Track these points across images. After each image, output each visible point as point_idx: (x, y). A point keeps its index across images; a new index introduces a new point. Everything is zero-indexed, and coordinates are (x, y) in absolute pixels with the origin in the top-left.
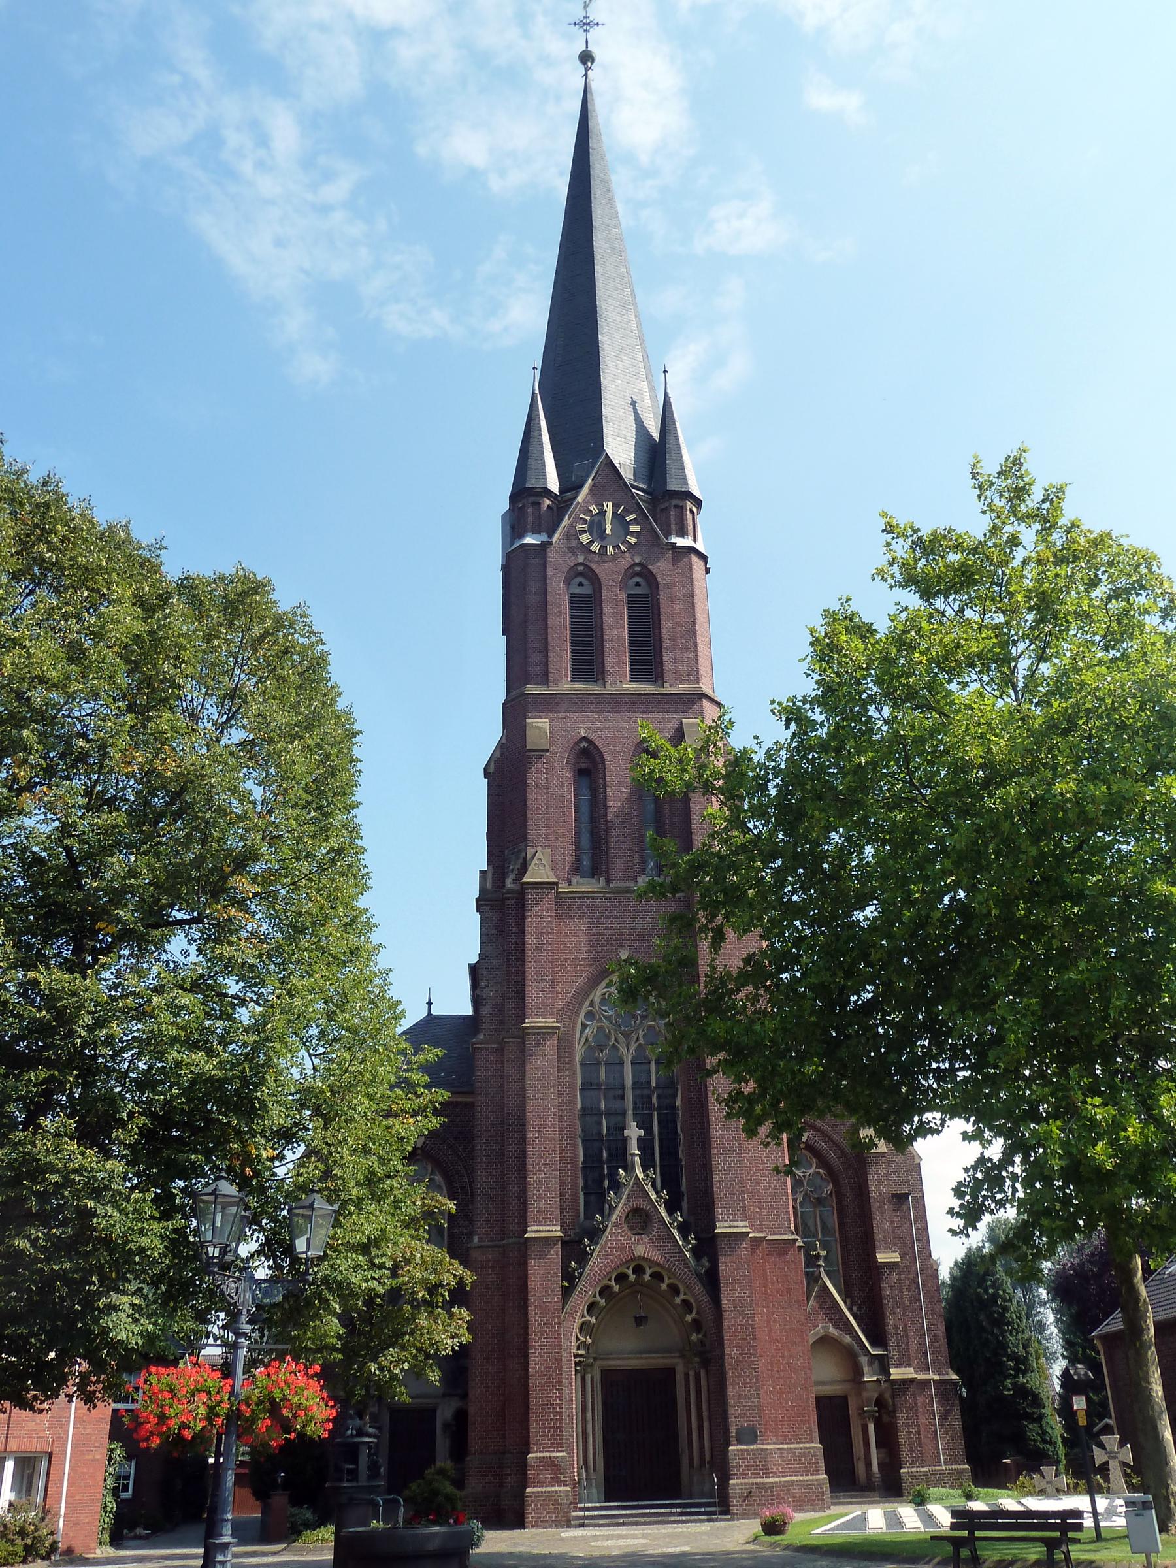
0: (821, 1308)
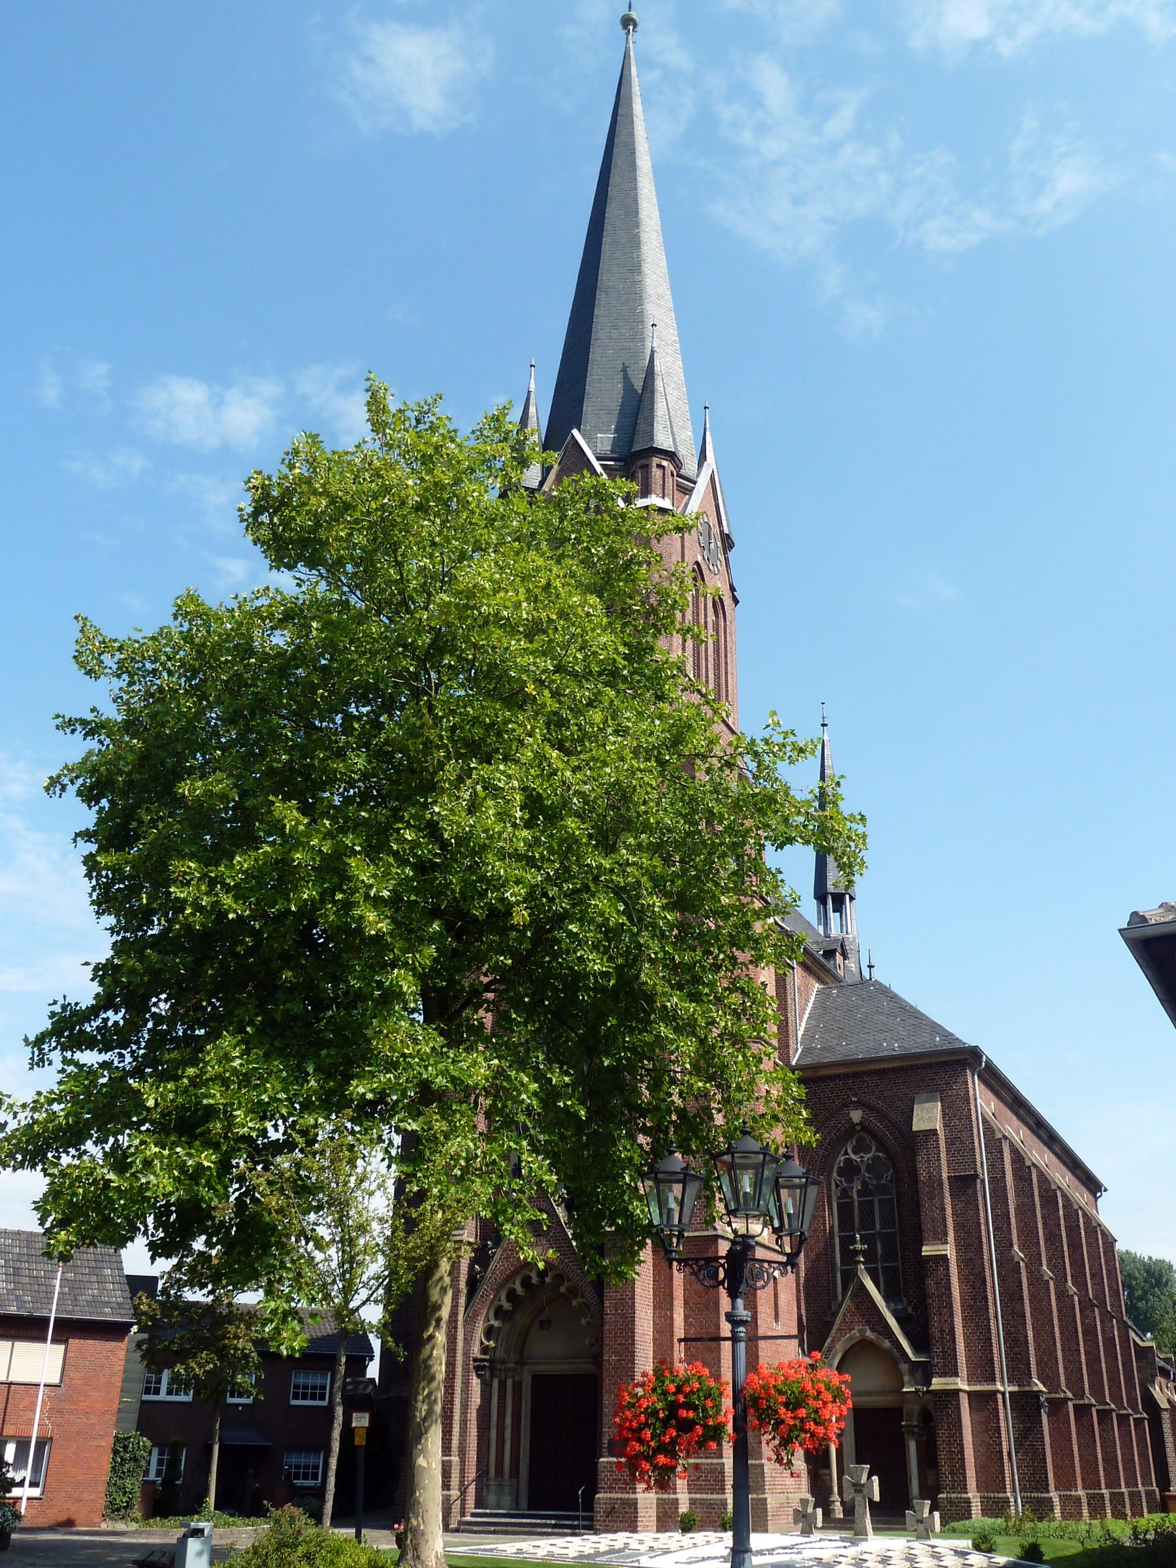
0: (857, 1309)
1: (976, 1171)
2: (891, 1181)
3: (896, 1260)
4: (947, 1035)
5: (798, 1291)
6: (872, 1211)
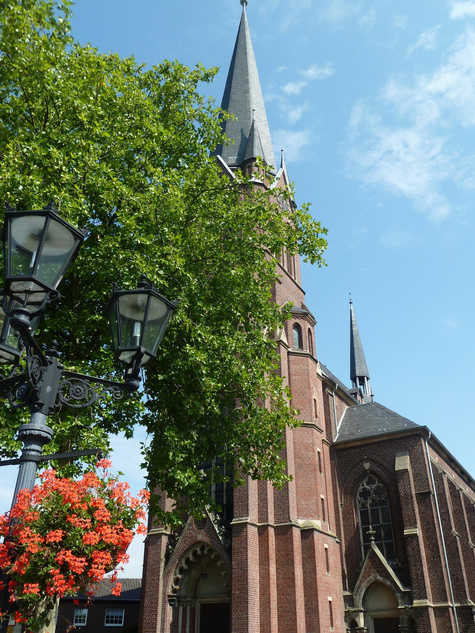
0: (373, 565)
1: (429, 490)
2: (387, 498)
3: (391, 539)
4: (410, 423)
5: (341, 557)
6: (378, 514)
